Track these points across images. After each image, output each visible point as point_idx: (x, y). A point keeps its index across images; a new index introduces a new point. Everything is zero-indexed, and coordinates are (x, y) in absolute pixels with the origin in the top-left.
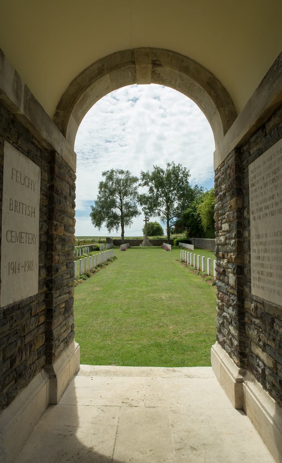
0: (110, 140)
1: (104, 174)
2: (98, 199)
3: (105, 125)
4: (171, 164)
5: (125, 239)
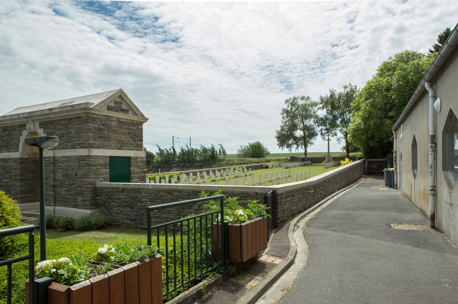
0: (337, 43)
1: (287, 101)
2: (282, 123)
3: (329, 26)
4: (347, 86)
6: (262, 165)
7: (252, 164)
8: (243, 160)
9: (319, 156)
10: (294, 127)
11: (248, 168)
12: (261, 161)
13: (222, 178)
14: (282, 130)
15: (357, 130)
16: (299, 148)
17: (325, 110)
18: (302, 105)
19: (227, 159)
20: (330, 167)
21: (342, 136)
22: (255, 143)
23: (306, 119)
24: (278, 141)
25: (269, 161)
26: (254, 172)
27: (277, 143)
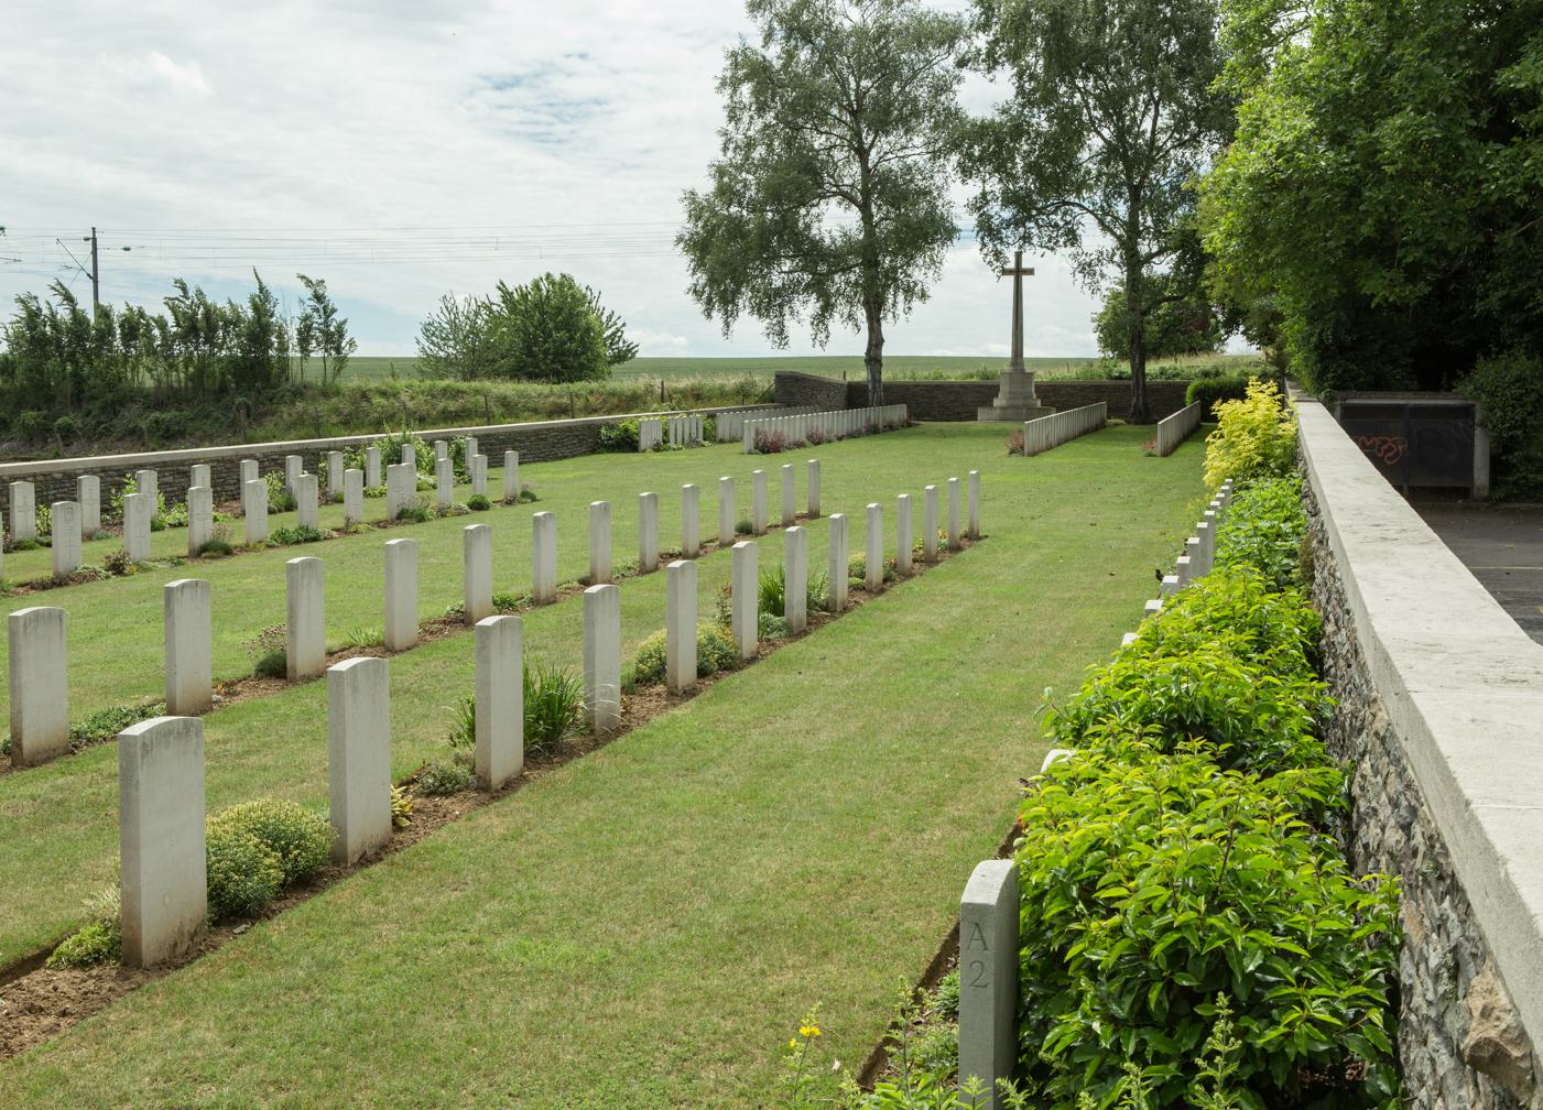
1: (563, 276)
2: (725, 149)
5: (886, 376)
6: (593, 429)
7: (517, 418)
8: (458, 393)
9: (954, 376)
10: (801, 180)
11: (493, 448)
12: (579, 404)
13: (289, 522)
14: (726, 193)
15: (1283, 186)
16: (836, 324)
17: (1006, 73)
18: (860, 32)
19: (351, 382)
20: (1050, 448)
21: (1109, 243)
22: (544, 286)
23: (882, 126)
24: (700, 264)
25: (632, 402)
26: (544, 476)
27: (689, 281)
